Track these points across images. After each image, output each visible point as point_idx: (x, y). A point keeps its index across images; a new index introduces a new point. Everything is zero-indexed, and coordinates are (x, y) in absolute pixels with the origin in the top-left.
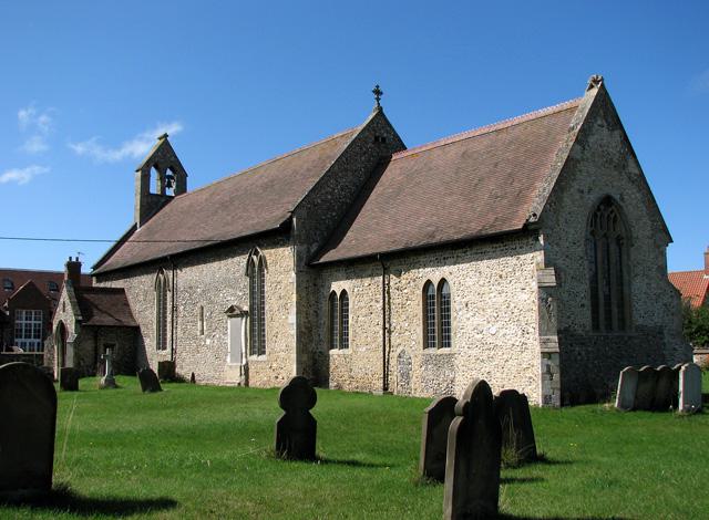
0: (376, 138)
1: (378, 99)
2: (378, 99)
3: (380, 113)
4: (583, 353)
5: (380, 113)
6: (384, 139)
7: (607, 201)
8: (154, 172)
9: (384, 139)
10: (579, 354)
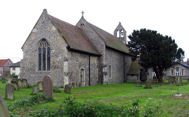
0: (81, 24)
1: (83, 14)
2: (83, 14)
3: (82, 17)
5: (82, 17)
6: (83, 24)
8: (118, 32)
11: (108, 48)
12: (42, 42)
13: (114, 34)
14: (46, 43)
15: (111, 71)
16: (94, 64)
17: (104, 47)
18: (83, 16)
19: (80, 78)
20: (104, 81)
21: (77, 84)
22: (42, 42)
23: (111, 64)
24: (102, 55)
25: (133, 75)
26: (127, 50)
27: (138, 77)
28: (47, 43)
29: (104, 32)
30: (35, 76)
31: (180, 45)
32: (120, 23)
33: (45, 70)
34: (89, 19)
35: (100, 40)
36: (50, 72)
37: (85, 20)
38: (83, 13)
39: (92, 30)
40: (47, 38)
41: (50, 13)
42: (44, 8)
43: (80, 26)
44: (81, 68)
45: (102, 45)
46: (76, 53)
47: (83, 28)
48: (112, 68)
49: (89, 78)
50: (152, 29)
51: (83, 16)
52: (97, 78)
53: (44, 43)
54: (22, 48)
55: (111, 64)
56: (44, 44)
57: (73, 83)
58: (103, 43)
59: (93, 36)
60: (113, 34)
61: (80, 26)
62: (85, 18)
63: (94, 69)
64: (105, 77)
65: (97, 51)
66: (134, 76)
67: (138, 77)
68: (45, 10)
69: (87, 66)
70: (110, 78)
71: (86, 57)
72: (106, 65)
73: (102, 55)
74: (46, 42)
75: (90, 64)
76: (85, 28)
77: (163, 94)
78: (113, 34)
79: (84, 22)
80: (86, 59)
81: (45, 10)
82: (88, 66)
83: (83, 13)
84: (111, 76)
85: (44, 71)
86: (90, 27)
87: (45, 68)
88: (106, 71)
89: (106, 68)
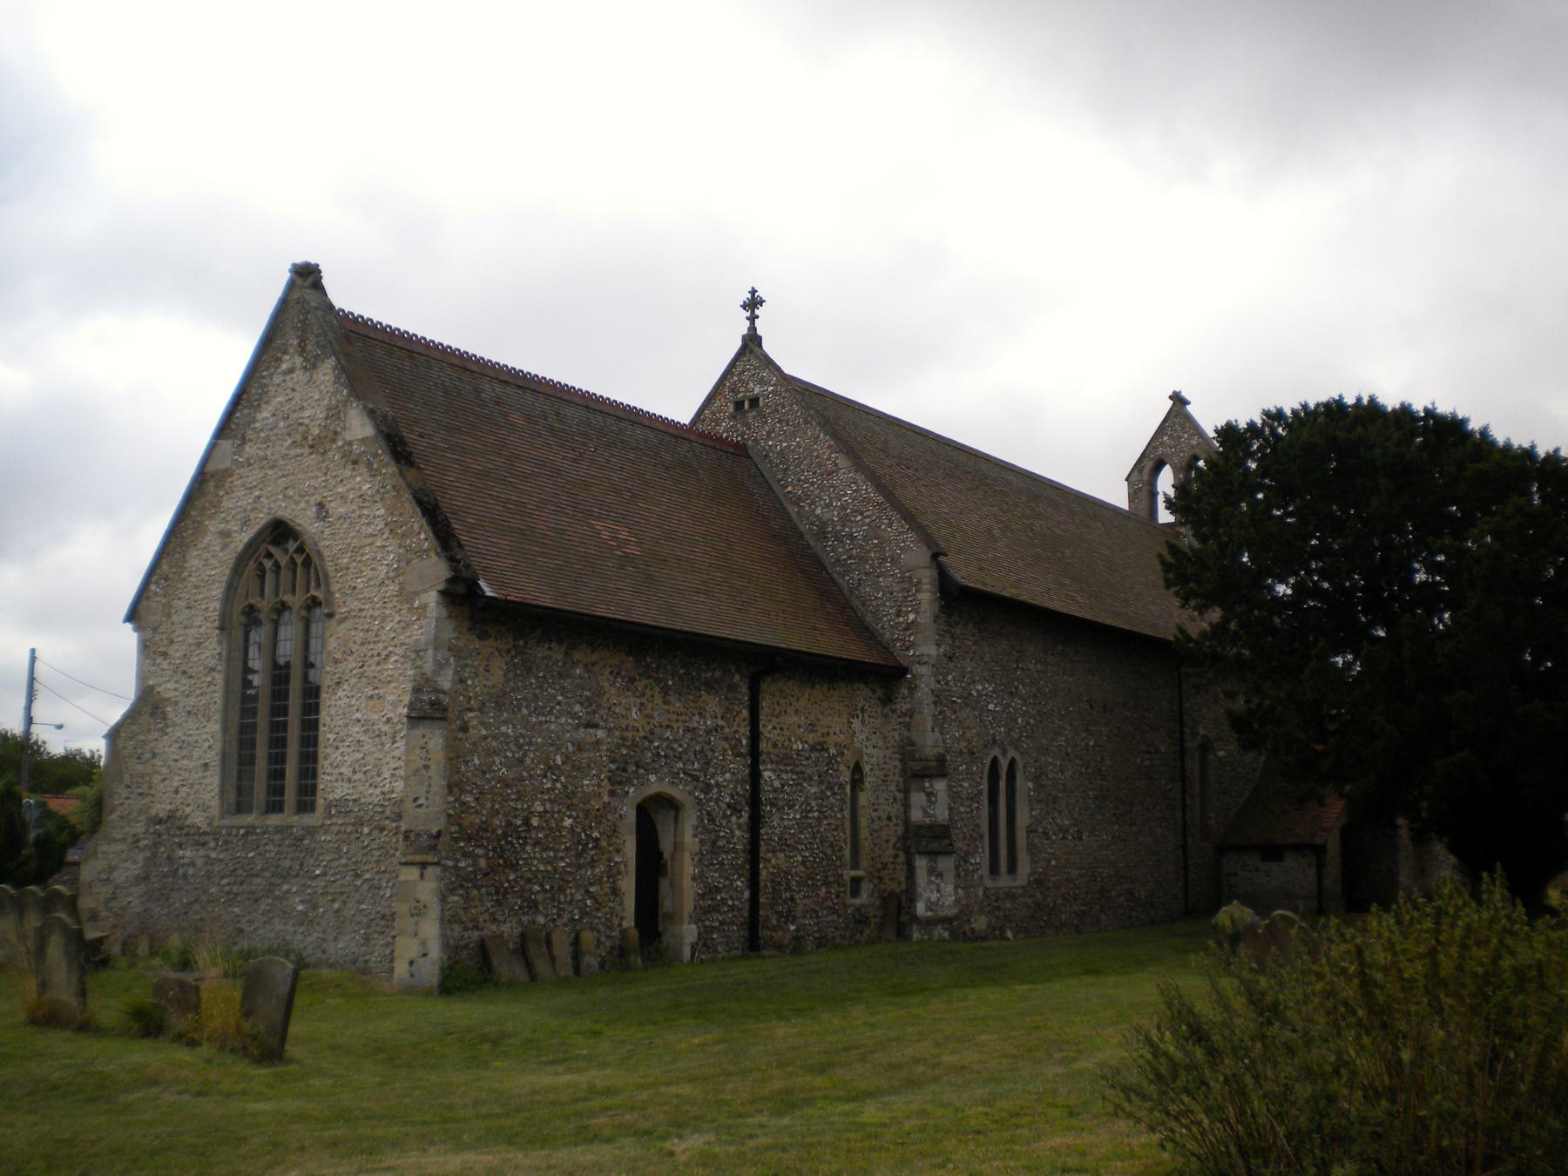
0: (739, 405)
1: (753, 318)
2: (753, 318)
3: (752, 341)
4: (199, 862)
5: (752, 341)
6: (754, 402)
7: (280, 531)
9: (754, 402)
10: (193, 864)
11: (959, 601)
12: (269, 555)
13: (1133, 496)
14: (299, 560)
15: (1022, 820)
16: (820, 747)
17: (926, 597)
18: (753, 328)
19: (628, 885)
20: (921, 909)
21: (576, 943)
22: (269, 555)
23: (1012, 753)
24: (905, 670)
25: (1272, 853)
26: (1164, 614)
27: (1320, 866)
28: (308, 562)
29: (1011, 477)
30: (209, 861)
31: (313, 262)
32: (1178, 400)
33: (275, 807)
34: (798, 355)
35: (893, 527)
36: (311, 831)
37: (769, 363)
38: (753, 303)
39: (823, 447)
40: (304, 518)
41: (345, 294)
42: (299, 260)
43: (733, 417)
44: (635, 794)
45: (909, 582)
46: (572, 647)
47: (771, 448)
48: (1024, 785)
49: (754, 883)
50: (1317, 395)
51: (753, 328)
52: (856, 882)
53: (283, 561)
54: (133, 616)
55: (1012, 753)
56: (269, 577)
57: (523, 936)
58: (916, 556)
59: (833, 496)
60: (1118, 497)
61: (733, 417)
62: (767, 347)
63: (821, 796)
64: (931, 871)
65: (867, 634)
66: (1290, 861)
67: (1320, 866)
68: (307, 277)
69: (730, 775)
70: (1004, 881)
71: (710, 686)
72: (941, 760)
73: (905, 670)
74: (300, 550)
75: (763, 745)
76: (772, 438)
77: (385, 1164)
78: (1118, 497)
79: (762, 382)
80: (712, 703)
81: (307, 277)
82: (740, 767)
83: (753, 303)
84: (1024, 859)
85: (274, 820)
86: (827, 424)
87: (280, 791)
88: (941, 814)
89: (940, 786)
